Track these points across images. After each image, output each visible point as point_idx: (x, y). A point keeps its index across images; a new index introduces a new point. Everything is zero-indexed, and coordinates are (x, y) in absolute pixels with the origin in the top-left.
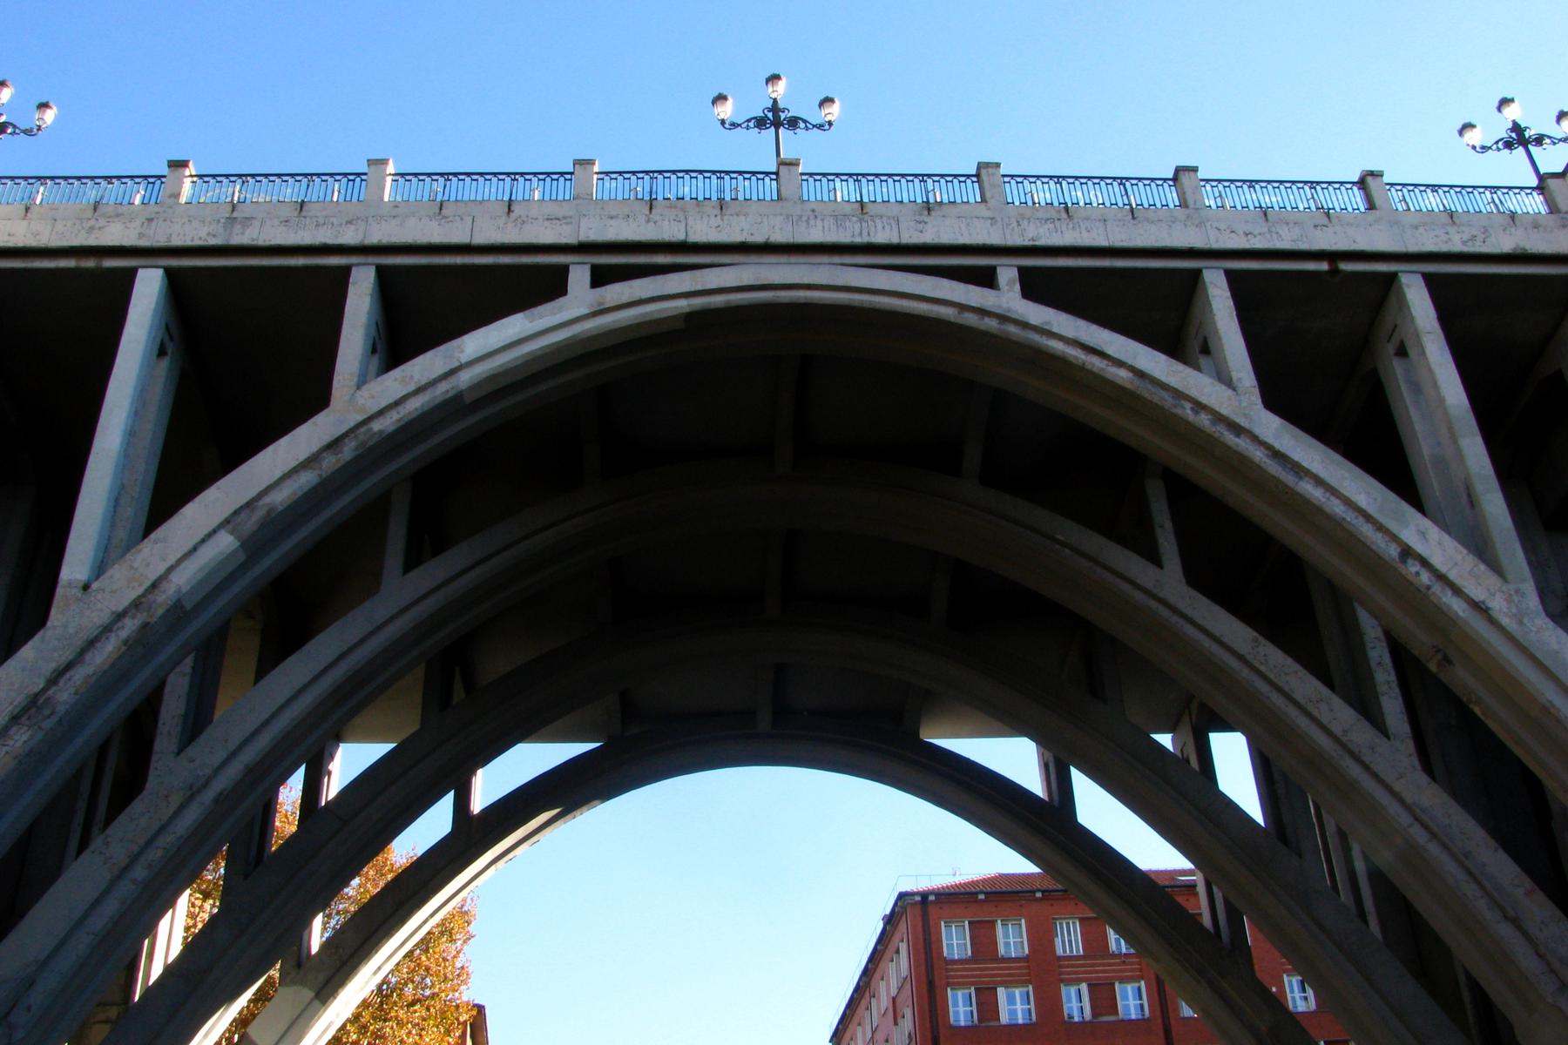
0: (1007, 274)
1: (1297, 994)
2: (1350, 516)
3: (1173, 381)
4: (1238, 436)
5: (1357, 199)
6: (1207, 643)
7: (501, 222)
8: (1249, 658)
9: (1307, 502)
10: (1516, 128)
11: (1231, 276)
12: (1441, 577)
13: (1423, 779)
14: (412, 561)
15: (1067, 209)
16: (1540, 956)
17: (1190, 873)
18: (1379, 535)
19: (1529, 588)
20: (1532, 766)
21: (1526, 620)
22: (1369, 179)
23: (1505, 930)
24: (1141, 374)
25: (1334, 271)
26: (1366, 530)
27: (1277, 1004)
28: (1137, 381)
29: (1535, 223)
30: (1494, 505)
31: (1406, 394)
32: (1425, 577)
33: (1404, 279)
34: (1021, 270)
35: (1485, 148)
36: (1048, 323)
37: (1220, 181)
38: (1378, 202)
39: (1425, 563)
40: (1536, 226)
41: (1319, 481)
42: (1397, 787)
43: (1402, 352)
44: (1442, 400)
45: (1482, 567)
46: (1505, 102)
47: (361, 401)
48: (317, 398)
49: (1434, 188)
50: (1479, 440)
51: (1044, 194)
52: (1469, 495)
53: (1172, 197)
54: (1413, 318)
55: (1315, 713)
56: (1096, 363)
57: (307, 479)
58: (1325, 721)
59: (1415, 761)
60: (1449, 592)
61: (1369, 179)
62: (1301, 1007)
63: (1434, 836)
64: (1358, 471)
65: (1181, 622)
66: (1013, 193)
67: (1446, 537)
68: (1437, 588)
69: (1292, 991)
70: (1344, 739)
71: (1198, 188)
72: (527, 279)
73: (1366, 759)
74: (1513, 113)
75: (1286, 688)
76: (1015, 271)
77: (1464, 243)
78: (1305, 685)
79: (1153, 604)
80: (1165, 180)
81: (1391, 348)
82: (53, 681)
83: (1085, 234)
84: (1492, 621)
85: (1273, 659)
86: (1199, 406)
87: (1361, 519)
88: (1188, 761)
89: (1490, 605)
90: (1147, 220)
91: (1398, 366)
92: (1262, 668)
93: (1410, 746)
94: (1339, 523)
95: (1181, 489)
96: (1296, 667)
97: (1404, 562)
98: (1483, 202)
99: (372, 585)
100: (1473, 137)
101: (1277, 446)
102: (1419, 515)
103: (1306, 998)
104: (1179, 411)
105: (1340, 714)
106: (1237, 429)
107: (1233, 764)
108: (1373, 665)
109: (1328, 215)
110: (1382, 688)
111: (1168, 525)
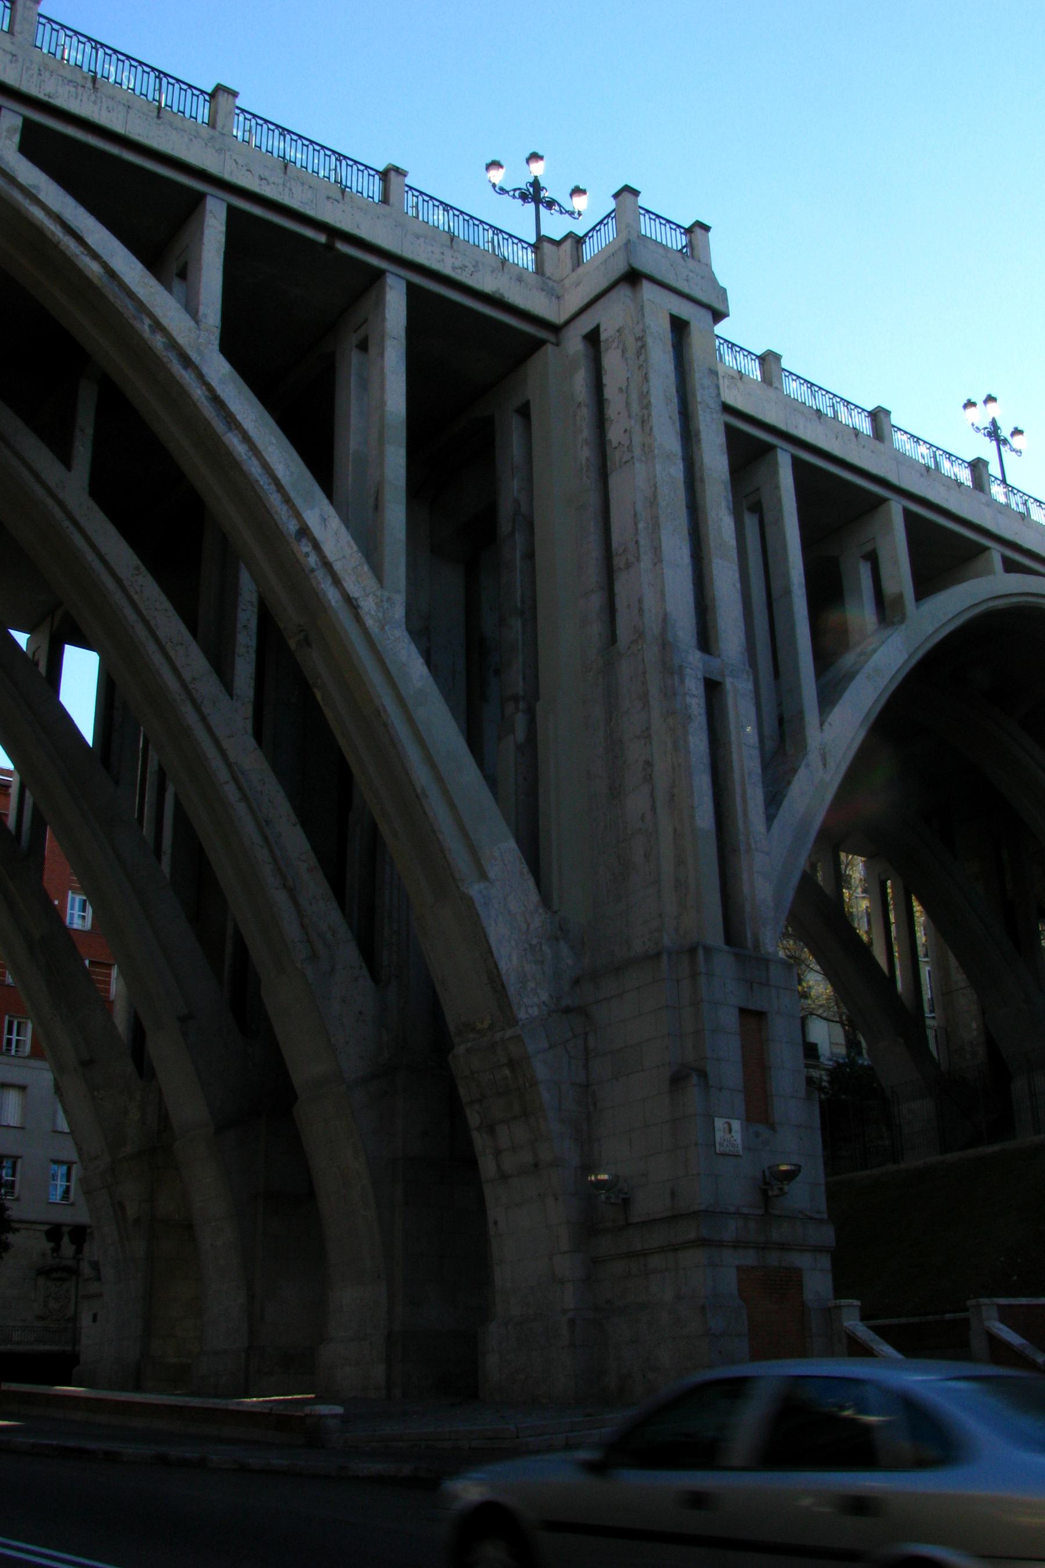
1: (77, 912)
2: (263, 481)
3: (141, 292)
4: (185, 368)
5: (374, 188)
6: (90, 556)
8: (126, 583)
9: (229, 453)
10: (536, 184)
11: (233, 213)
12: (327, 565)
13: (251, 742)
15: (94, 79)
16: (302, 926)
17: (7, 772)
18: (285, 508)
19: (400, 600)
20: (350, 758)
21: (387, 628)
22: (393, 174)
23: (281, 898)
24: (112, 274)
25: (329, 247)
26: (274, 499)
27: (56, 916)
28: (106, 279)
29: (520, 276)
30: (395, 514)
31: (353, 386)
32: (313, 560)
33: (390, 280)
34: (27, 123)
35: (503, 191)
36: (36, 187)
37: (255, 116)
38: (393, 199)
39: (317, 546)
40: (520, 279)
41: (246, 438)
42: (226, 744)
43: (363, 346)
44: (383, 403)
45: (366, 568)
46: (535, 157)
49: (447, 207)
50: (402, 452)
51: (75, 53)
52: (377, 499)
53: (203, 112)
54: (384, 319)
55: (172, 654)
58: (178, 665)
59: (249, 725)
60: (329, 581)
61: (393, 174)
62: (77, 924)
63: (244, 798)
64: (286, 442)
65: (72, 529)
66: (45, 38)
67: (343, 529)
68: (320, 574)
69: (72, 908)
70: (191, 686)
71: (230, 114)
73: (206, 711)
74: (537, 169)
75: (152, 623)
76: (19, 122)
77: (454, 268)
78: (170, 625)
79: (50, 502)
80: (202, 92)
81: (354, 339)
83: (104, 113)
84: (358, 619)
85: (149, 591)
86: (158, 326)
87: (273, 487)
88: (37, 664)
89: (362, 604)
90: (171, 125)
91: (355, 357)
92: (136, 597)
93: (249, 710)
94: (251, 484)
95: (114, 403)
96: (167, 605)
97: (299, 541)
98: (483, 238)
100: (497, 176)
101: (219, 392)
102: (326, 501)
103: (84, 917)
104: (137, 324)
105: (194, 662)
106: (187, 361)
107: (79, 681)
108: (239, 626)
109: (343, 192)
110: (240, 650)
111: (90, 431)
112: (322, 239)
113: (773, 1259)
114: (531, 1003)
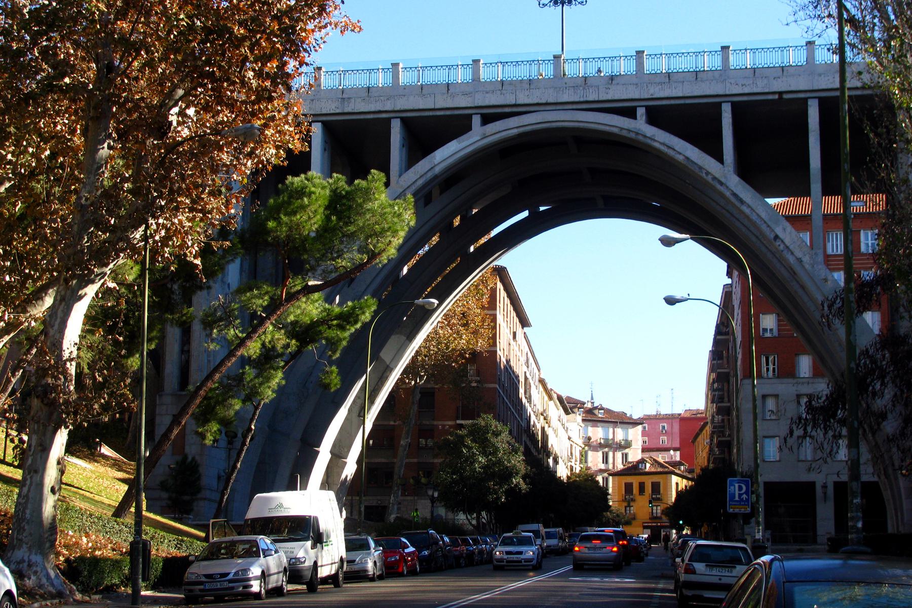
0: (641, 112)
3: (699, 162)
7: (445, 96)
33: (810, 102)
47: (401, 183)
56: (671, 153)
89: (803, 259)
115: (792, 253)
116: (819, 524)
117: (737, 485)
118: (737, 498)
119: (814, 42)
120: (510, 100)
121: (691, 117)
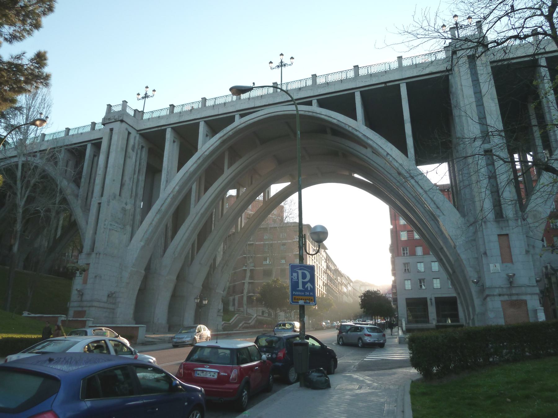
14: (230, 165)
32: (391, 159)
33: (401, 85)
48: (196, 150)
57: (195, 165)
68: (393, 161)
72: (230, 119)
82: (162, 206)
99: (222, 172)
100: (273, 65)
112: (383, 85)
113: (514, 298)
114: (460, 242)
115: (397, 162)
116: (429, 315)
117: (300, 272)
118: (301, 287)
119: (401, 57)
120: (252, 105)
121: (339, 100)
